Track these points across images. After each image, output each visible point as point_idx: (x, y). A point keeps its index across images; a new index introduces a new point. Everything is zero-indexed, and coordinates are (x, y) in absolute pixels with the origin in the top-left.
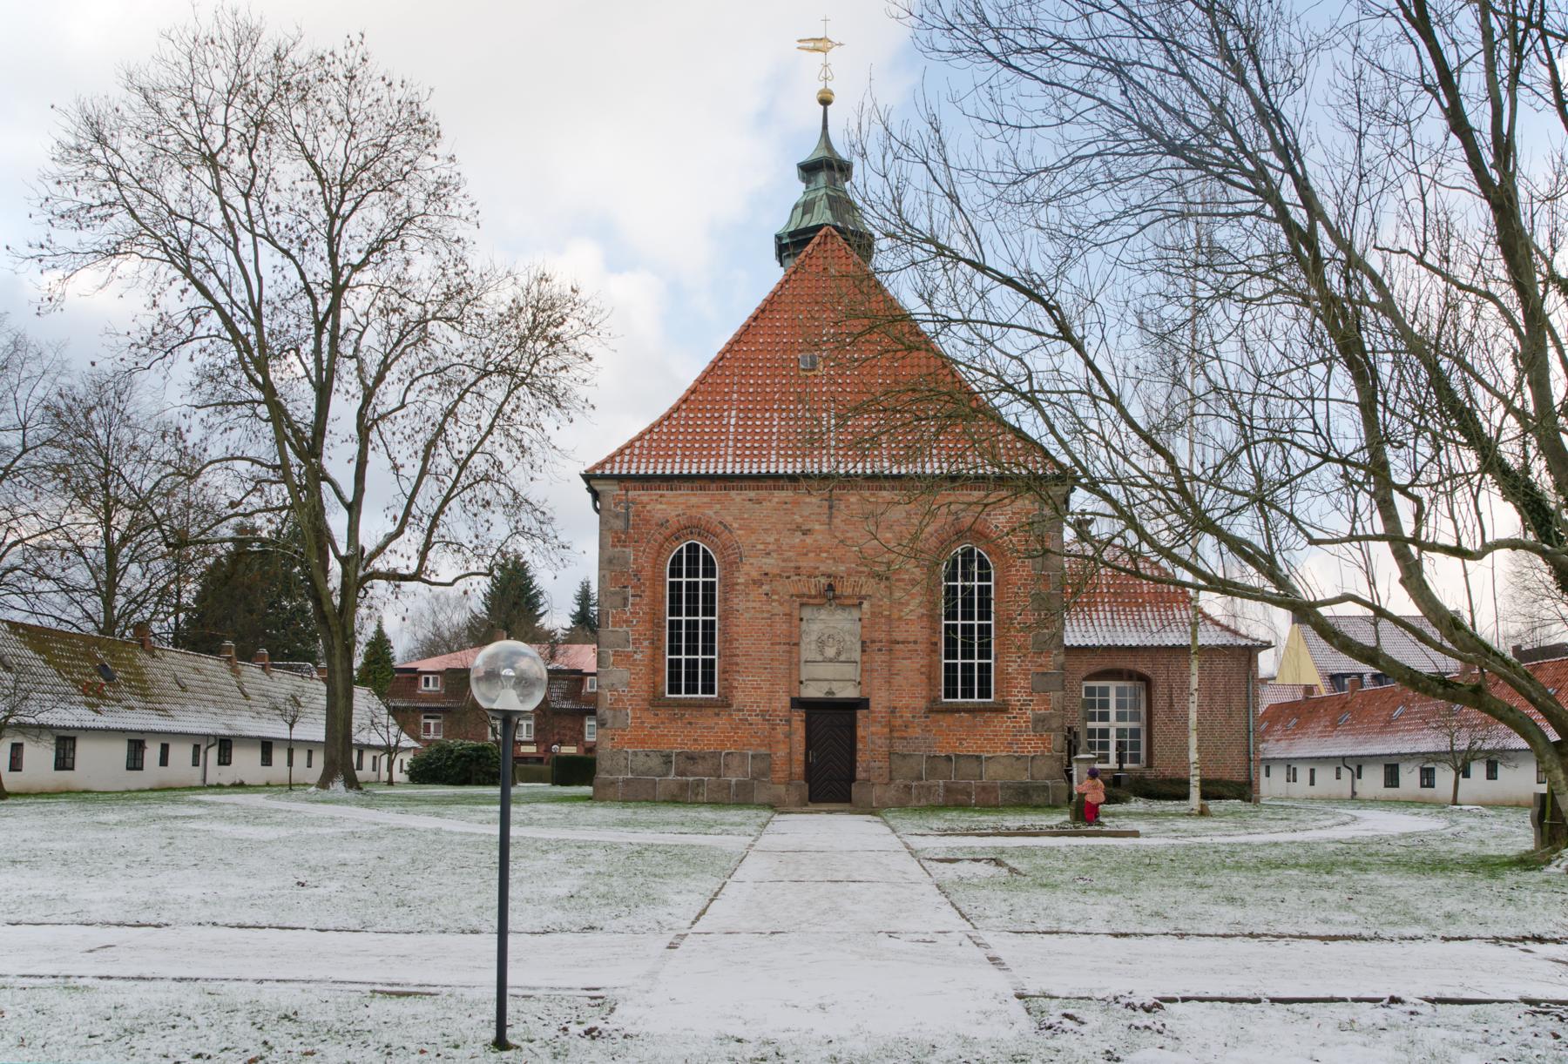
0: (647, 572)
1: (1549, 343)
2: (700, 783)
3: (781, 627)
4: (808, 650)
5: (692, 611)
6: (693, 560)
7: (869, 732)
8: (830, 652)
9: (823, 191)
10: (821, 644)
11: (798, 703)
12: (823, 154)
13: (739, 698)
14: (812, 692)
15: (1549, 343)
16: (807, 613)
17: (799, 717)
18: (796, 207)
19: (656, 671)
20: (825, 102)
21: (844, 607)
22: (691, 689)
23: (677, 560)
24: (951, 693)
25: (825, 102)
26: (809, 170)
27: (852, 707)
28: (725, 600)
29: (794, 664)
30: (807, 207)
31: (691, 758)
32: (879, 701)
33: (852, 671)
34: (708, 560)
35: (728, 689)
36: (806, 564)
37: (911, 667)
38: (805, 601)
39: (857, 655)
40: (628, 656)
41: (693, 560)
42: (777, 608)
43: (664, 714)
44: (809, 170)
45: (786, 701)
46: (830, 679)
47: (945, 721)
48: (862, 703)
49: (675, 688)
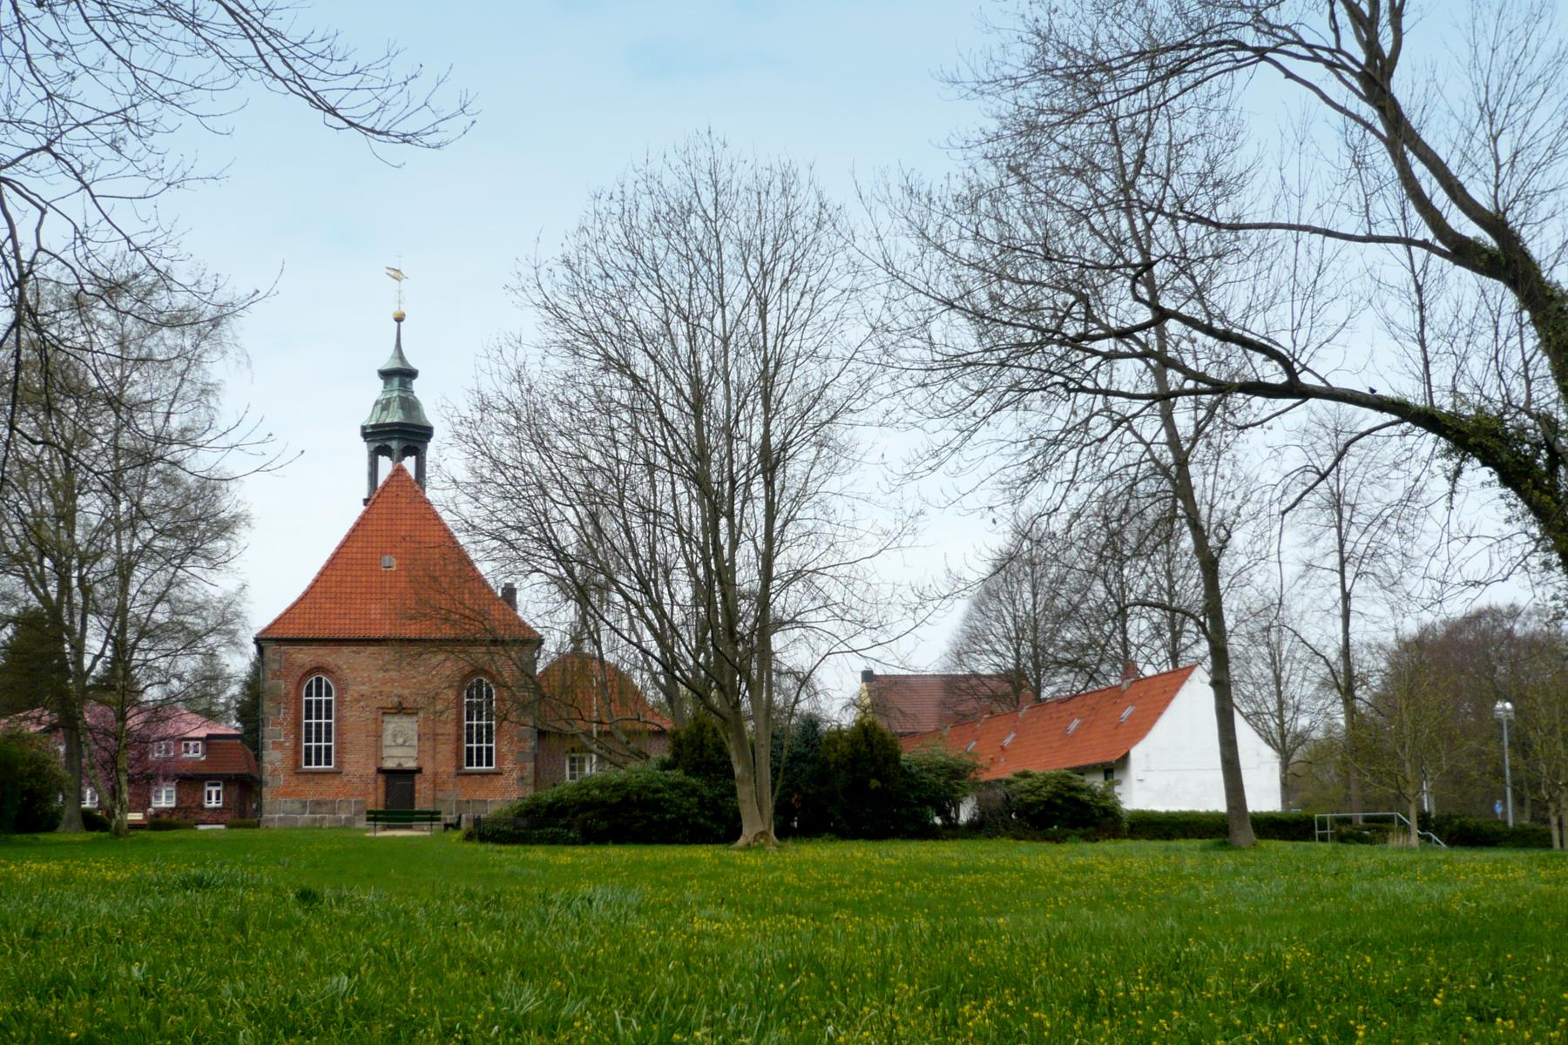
0: (292, 694)
1: (1438, 244)
2: (323, 819)
3: (372, 727)
4: (387, 739)
5: (319, 717)
6: (319, 687)
7: (423, 789)
8: (400, 741)
9: (396, 394)
10: (395, 736)
11: (380, 771)
12: (396, 365)
13: (347, 768)
14: (390, 764)
15: (1438, 244)
16: (387, 718)
17: (381, 779)
18: (377, 403)
19: (297, 752)
20: (399, 319)
21: (408, 714)
22: (479, 763)
23: (310, 687)
24: (470, 763)
25: (399, 319)
26: (386, 375)
27: (410, 774)
28: (338, 710)
29: (378, 748)
30: (385, 406)
31: (318, 803)
32: (428, 769)
33: (414, 752)
34: (328, 687)
35: (340, 763)
36: (386, 689)
37: (446, 750)
38: (386, 712)
39: (415, 742)
40: (281, 744)
41: (319, 687)
42: (367, 715)
43: (302, 778)
44: (386, 375)
45: (373, 769)
46: (400, 755)
47: (466, 780)
48: (419, 770)
49: (308, 763)
